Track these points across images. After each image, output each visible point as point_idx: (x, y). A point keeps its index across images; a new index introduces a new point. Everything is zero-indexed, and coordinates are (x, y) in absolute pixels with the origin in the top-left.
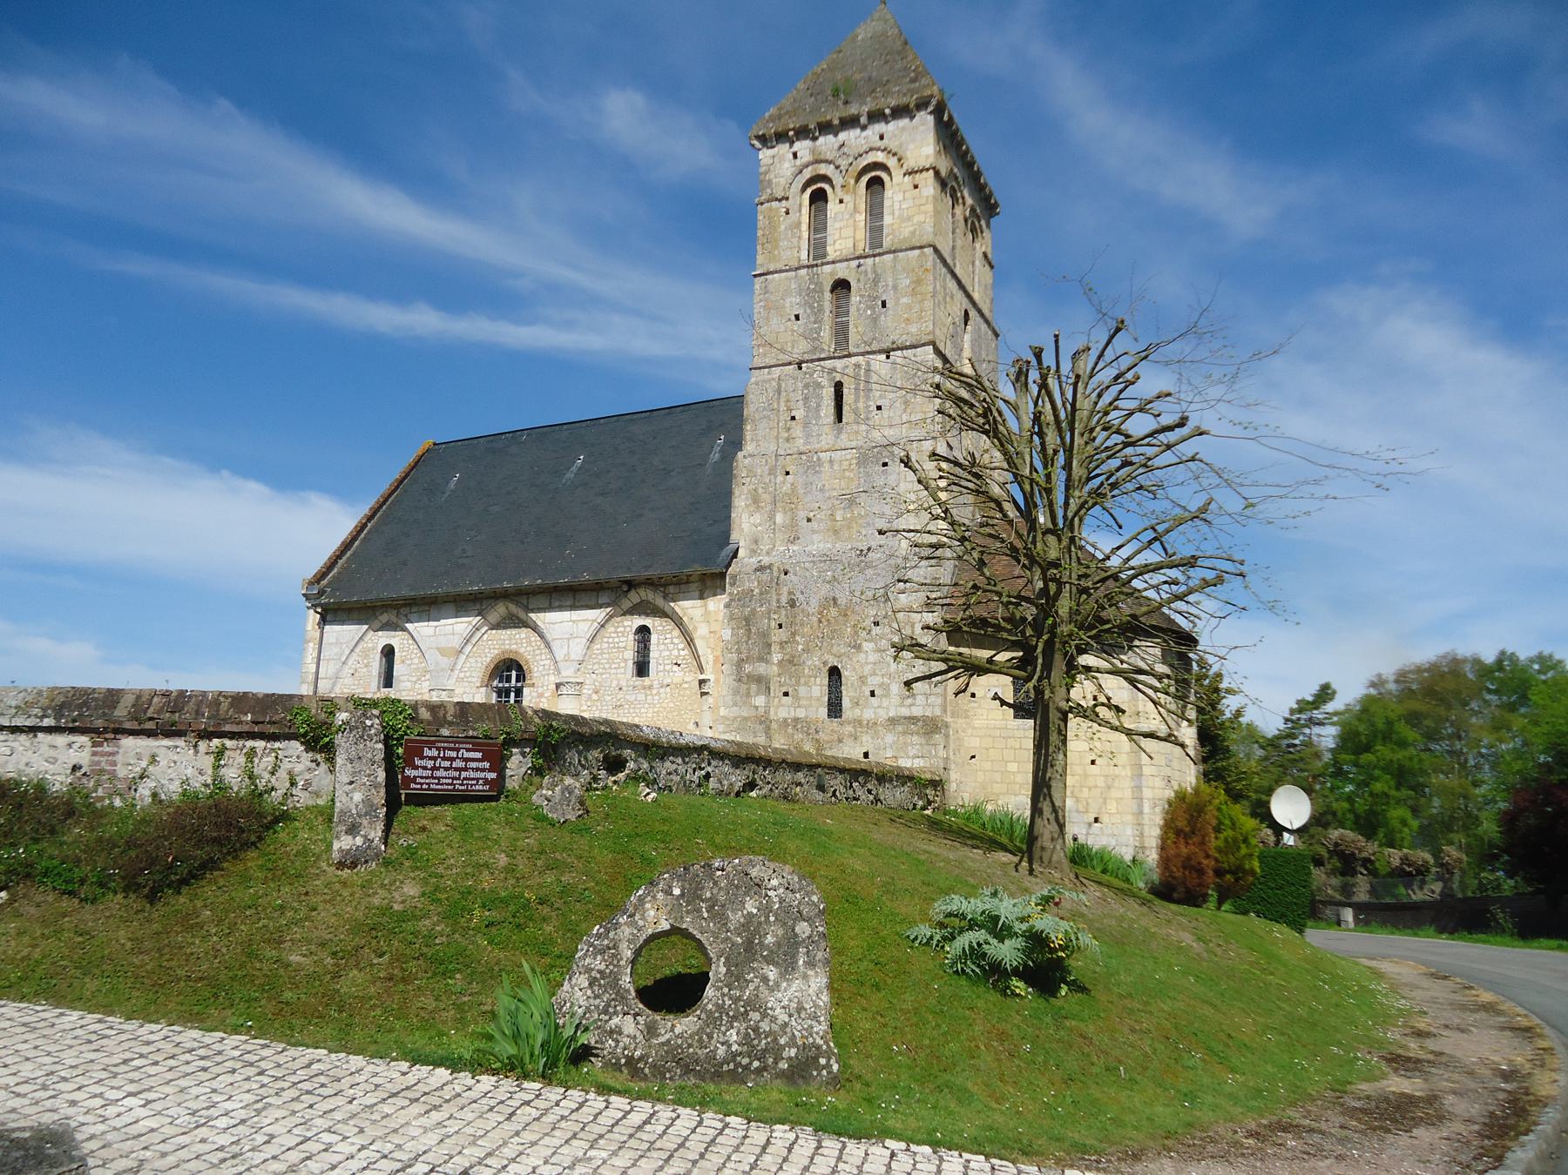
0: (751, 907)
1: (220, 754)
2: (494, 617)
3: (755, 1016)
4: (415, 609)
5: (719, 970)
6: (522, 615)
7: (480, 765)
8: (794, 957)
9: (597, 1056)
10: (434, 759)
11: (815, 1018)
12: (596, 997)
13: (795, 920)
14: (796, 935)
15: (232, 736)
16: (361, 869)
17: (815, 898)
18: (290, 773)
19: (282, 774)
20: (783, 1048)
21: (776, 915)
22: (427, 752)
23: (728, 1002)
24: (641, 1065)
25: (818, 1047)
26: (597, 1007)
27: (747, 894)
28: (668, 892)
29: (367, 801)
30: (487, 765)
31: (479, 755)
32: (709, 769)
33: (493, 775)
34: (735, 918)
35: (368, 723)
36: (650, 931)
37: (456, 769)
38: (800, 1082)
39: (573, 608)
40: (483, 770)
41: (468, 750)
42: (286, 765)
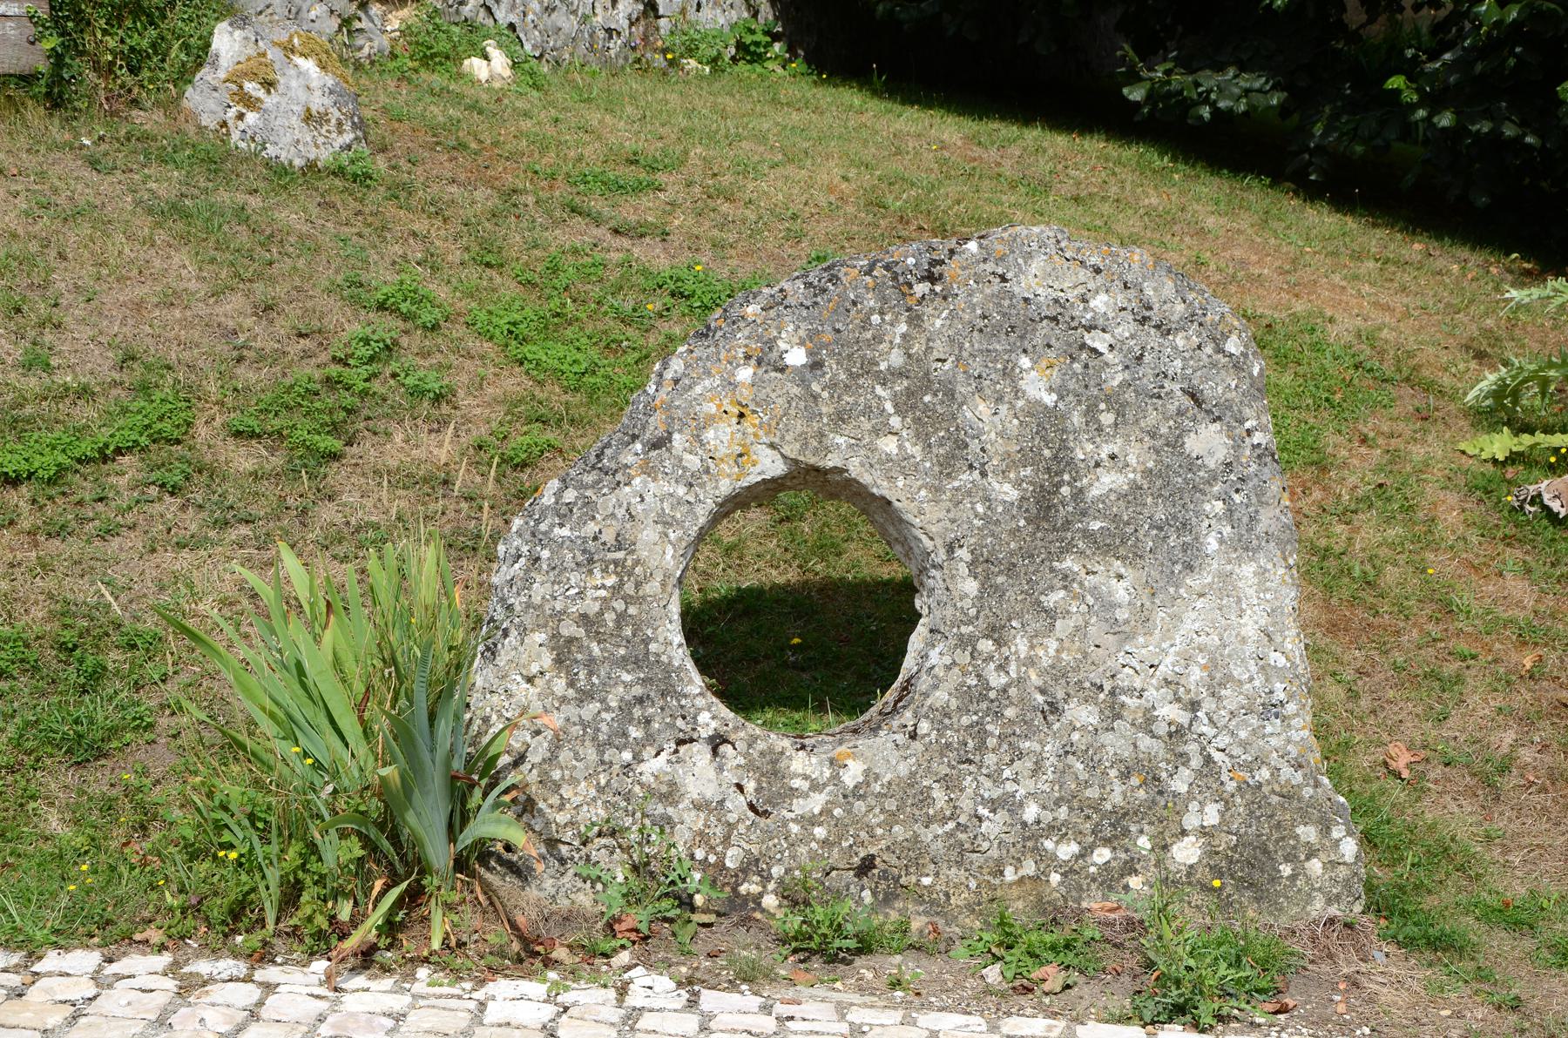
5: (951, 591)
11: (1271, 709)
12: (585, 696)
24: (749, 887)
36: (725, 487)
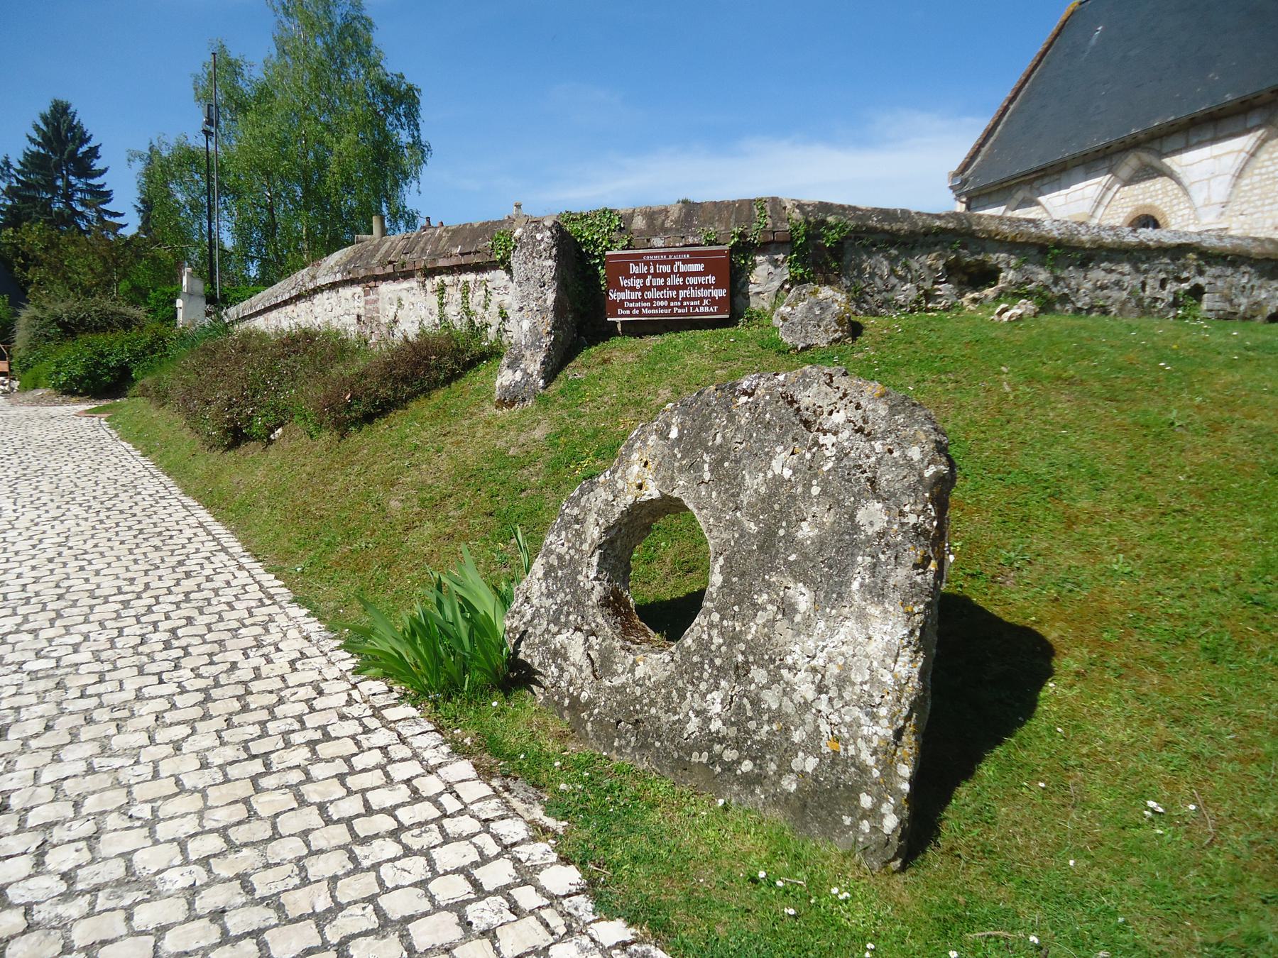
0: (781, 464)
1: (442, 289)
2: (1125, 171)
3: (759, 675)
4: (1046, 180)
6: (1155, 162)
7: (703, 280)
8: (844, 571)
9: (539, 684)
10: (643, 276)
13: (859, 496)
14: (856, 528)
15: (450, 270)
16: (518, 408)
17: (915, 453)
18: (500, 307)
19: (494, 308)
20: (793, 749)
21: (825, 484)
22: (634, 269)
23: (718, 640)
25: (863, 770)
26: (547, 610)
27: (780, 440)
28: (663, 435)
29: (534, 328)
30: (712, 279)
31: (699, 267)
32: (1201, 281)
33: (721, 293)
34: (754, 483)
35: (539, 237)
37: (672, 288)
38: (815, 828)
39: (1215, 140)
40: (707, 286)
41: (685, 262)
42: (496, 298)
